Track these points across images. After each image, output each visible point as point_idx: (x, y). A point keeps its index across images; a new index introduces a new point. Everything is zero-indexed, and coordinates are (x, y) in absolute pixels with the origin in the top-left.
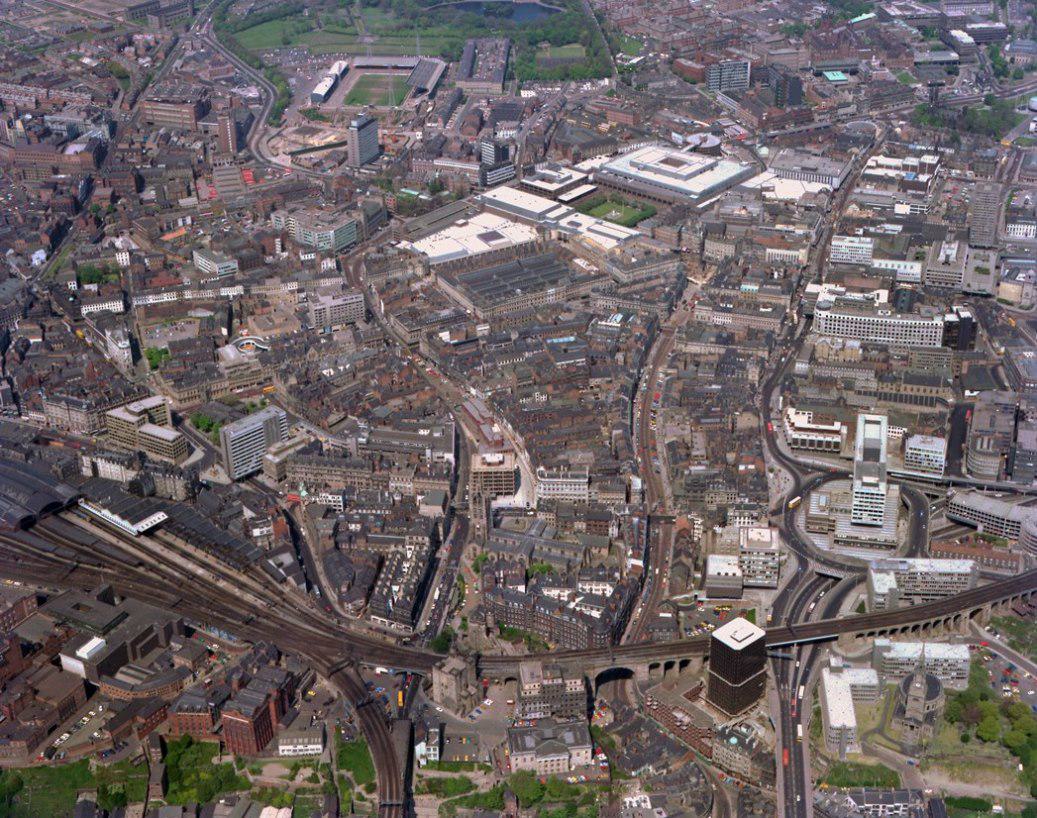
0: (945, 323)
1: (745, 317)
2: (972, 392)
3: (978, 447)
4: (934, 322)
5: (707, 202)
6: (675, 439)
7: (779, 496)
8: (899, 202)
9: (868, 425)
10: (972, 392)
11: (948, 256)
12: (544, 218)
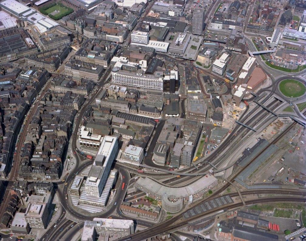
0: (163, 81)
1: (84, 72)
2: (168, 115)
3: (157, 151)
4: (159, 80)
5: (93, 8)
6: (28, 142)
7: (67, 172)
8: (170, 10)
9: (106, 143)
10: (168, 115)
11: (179, 42)
12: (22, 16)
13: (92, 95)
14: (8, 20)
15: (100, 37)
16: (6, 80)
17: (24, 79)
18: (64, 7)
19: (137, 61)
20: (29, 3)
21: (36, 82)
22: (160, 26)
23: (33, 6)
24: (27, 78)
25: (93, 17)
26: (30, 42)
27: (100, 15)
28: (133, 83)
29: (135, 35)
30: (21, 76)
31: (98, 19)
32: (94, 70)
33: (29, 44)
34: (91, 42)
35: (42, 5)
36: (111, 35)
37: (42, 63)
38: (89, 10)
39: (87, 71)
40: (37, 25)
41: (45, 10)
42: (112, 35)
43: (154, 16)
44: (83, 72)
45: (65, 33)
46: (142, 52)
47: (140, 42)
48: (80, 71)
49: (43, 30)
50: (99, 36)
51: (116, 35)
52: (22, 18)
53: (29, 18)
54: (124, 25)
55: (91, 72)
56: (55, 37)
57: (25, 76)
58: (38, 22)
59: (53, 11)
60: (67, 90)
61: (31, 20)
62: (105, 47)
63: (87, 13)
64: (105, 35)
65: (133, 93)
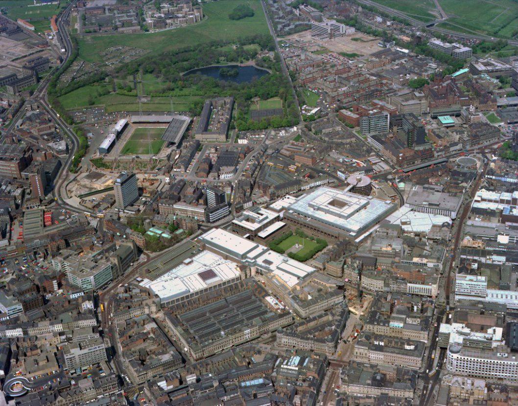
1: (394, 355)
12: (246, 257)
13: (419, 397)
14: (222, 267)
15: (395, 289)
16: (256, 378)
17: (289, 373)
18: (307, 237)
19: (483, 329)
20: (248, 235)
21: (314, 378)
22: (494, 263)
23: (255, 239)
24: (294, 372)
25: (371, 254)
26: (276, 304)
27: (384, 249)
28: (491, 370)
29: (463, 282)
30: (283, 368)
31: (379, 256)
32: (410, 350)
33: (276, 307)
34: (386, 299)
35: (270, 237)
36: (414, 283)
37: (310, 341)
38: (358, 240)
39: (398, 353)
40: (277, 272)
41: (278, 244)
42: (416, 283)
43: (474, 246)
44: (391, 354)
45: (331, 285)
46: (486, 313)
47: (473, 294)
48: (386, 354)
49: (292, 282)
50: (394, 287)
51: (423, 284)
52: (247, 261)
53: (260, 261)
54: (430, 265)
55: (406, 355)
56: (317, 294)
57: (289, 367)
58: (278, 268)
59: (290, 246)
60: (375, 392)
61: (263, 264)
62: (413, 307)
63: (355, 246)
64: (406, 284)
65: (498, 391)
